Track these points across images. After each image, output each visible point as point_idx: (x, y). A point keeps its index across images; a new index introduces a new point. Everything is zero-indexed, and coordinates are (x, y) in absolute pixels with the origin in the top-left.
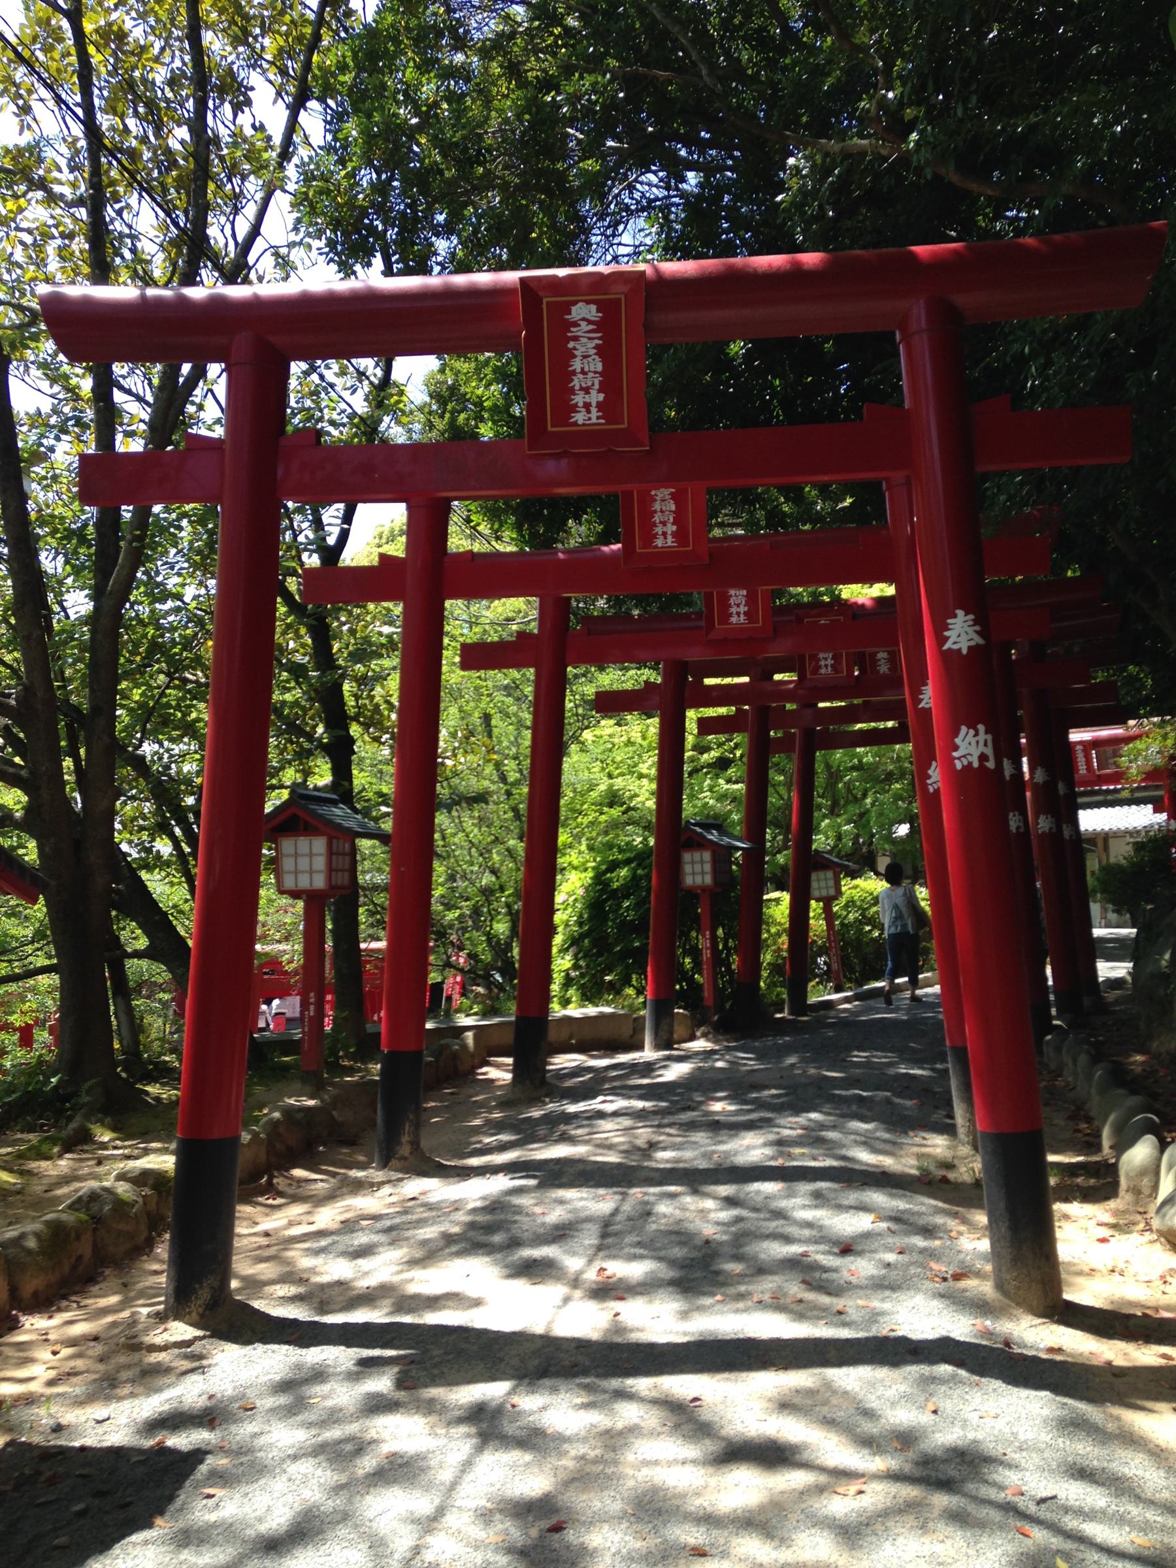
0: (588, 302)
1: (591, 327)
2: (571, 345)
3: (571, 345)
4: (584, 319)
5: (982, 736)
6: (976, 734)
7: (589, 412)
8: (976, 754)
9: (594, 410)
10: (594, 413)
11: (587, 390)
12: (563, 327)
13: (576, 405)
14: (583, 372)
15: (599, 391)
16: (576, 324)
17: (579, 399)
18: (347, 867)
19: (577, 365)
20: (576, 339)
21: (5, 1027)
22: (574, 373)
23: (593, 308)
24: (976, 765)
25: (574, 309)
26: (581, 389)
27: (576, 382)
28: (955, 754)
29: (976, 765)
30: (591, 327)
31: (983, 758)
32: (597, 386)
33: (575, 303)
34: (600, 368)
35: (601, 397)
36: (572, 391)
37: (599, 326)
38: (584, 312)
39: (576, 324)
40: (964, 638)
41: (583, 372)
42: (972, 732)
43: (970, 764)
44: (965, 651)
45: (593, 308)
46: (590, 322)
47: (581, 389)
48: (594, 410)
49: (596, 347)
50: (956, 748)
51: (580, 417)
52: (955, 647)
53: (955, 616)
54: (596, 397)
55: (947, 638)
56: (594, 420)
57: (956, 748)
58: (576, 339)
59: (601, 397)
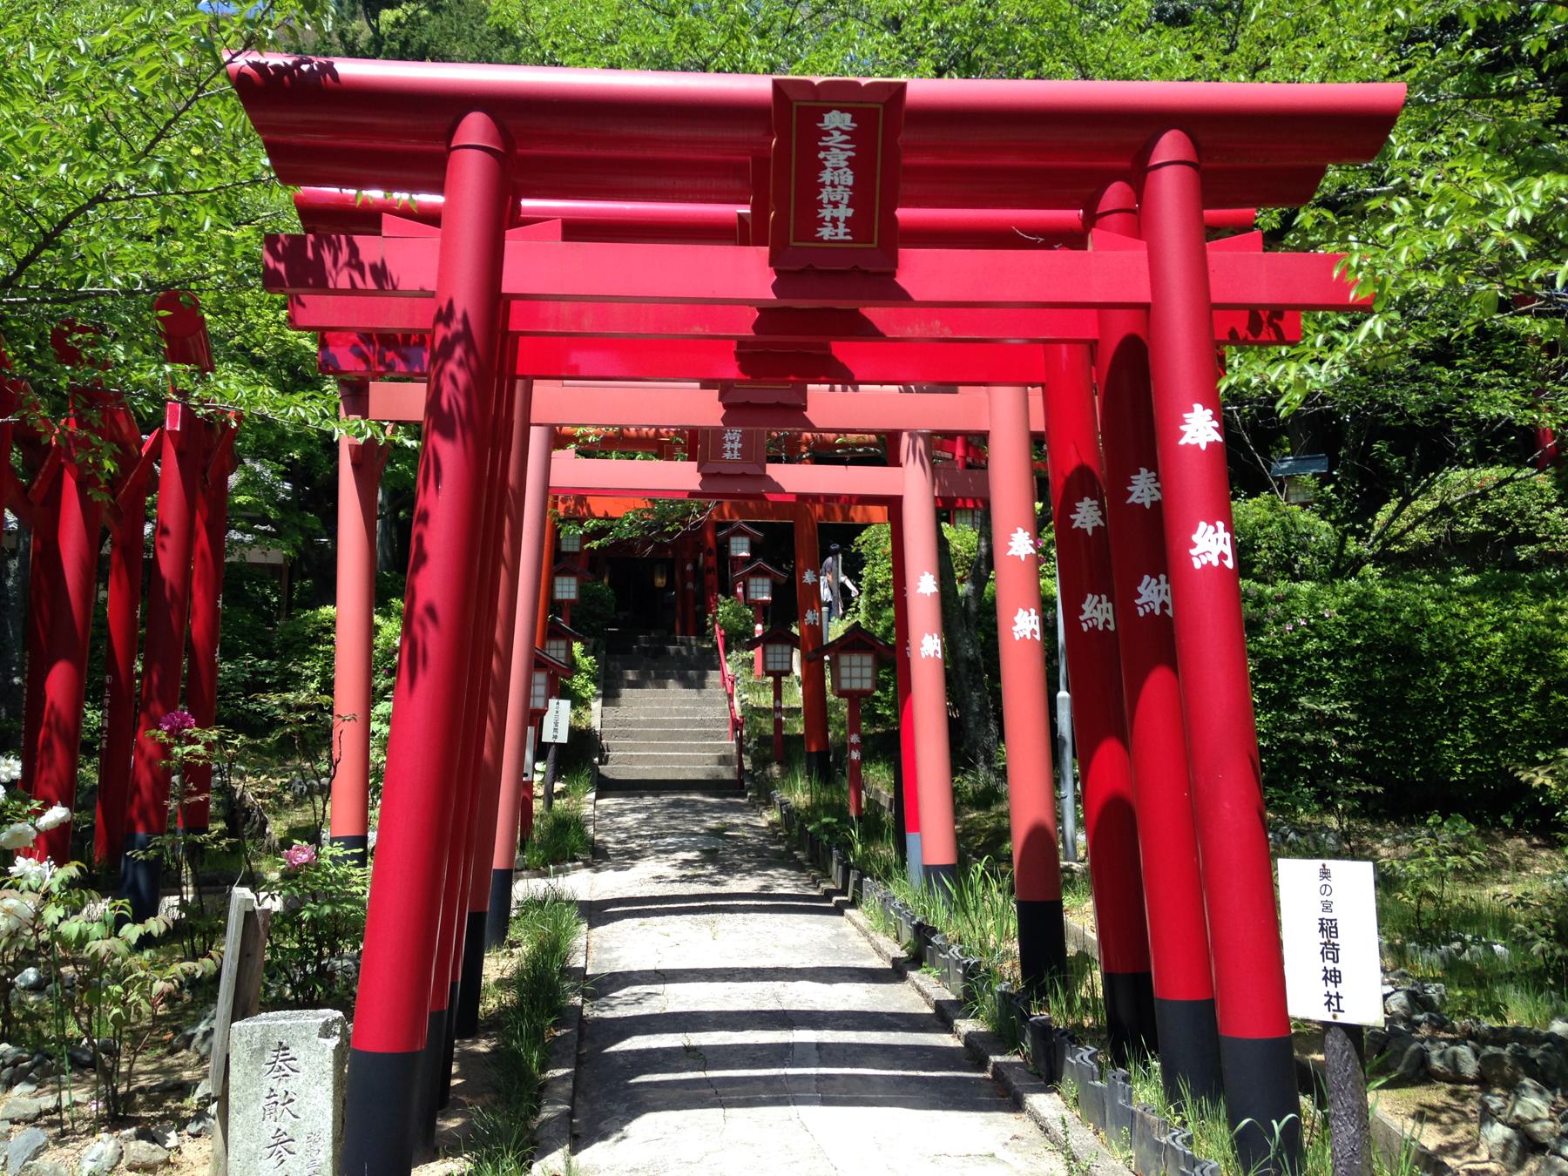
0: (843, 110)
1: (845, 137)
2: (822, 155)
3: (822, 155)
4: (837, 129)
5: (1164, 586)
6: (1100, 602)
7: (836, 227)
8: (1158, 602)
9: (841, 225)
10: (842, 229)
11: (835, 205)
12: (812, 137)
13: (823, 219)
14: (833, 185)
15: (848, 206)
16: (828, 134)
17: (827, 213)
18: (339, 286)
19: (826, 176)
20: (827, 149)
21: (1566, 413)
22: (823, 185)
23: (848, 117)
24: (1101, 628)
25: (827, 117)
26: (830, 202)
27: (825, 195)
28: (1138, 602)
29: (1157, 612)
30: (845, 137)
31: (1164, 605)
32: (846, 201)
33: (829, 110)
34: (850, 182)
35: (850, 212)
36: (820, 205)
37: (854, 136)
38: (837, 120)
39: (828, 134)
40: (1088, 520)
41: (833, 185)
42: (1154, 581)
43: (1152, 611)
44: (1148, 506)
45: (848, 117)
46: (843, 132)
47: (830, 202)
48: (841, 225)
49: (848, 159)
50: (1139, 596)
51: (826, 232)
52: (1139, 501)
53: (1138, 473)
54: (844, 212)
55: (1131, 493)
56: (841, 237)
57: (1139, 596)
58: (827, 149)
59: (850, 212)
